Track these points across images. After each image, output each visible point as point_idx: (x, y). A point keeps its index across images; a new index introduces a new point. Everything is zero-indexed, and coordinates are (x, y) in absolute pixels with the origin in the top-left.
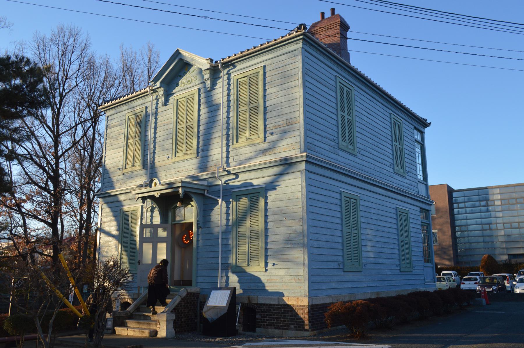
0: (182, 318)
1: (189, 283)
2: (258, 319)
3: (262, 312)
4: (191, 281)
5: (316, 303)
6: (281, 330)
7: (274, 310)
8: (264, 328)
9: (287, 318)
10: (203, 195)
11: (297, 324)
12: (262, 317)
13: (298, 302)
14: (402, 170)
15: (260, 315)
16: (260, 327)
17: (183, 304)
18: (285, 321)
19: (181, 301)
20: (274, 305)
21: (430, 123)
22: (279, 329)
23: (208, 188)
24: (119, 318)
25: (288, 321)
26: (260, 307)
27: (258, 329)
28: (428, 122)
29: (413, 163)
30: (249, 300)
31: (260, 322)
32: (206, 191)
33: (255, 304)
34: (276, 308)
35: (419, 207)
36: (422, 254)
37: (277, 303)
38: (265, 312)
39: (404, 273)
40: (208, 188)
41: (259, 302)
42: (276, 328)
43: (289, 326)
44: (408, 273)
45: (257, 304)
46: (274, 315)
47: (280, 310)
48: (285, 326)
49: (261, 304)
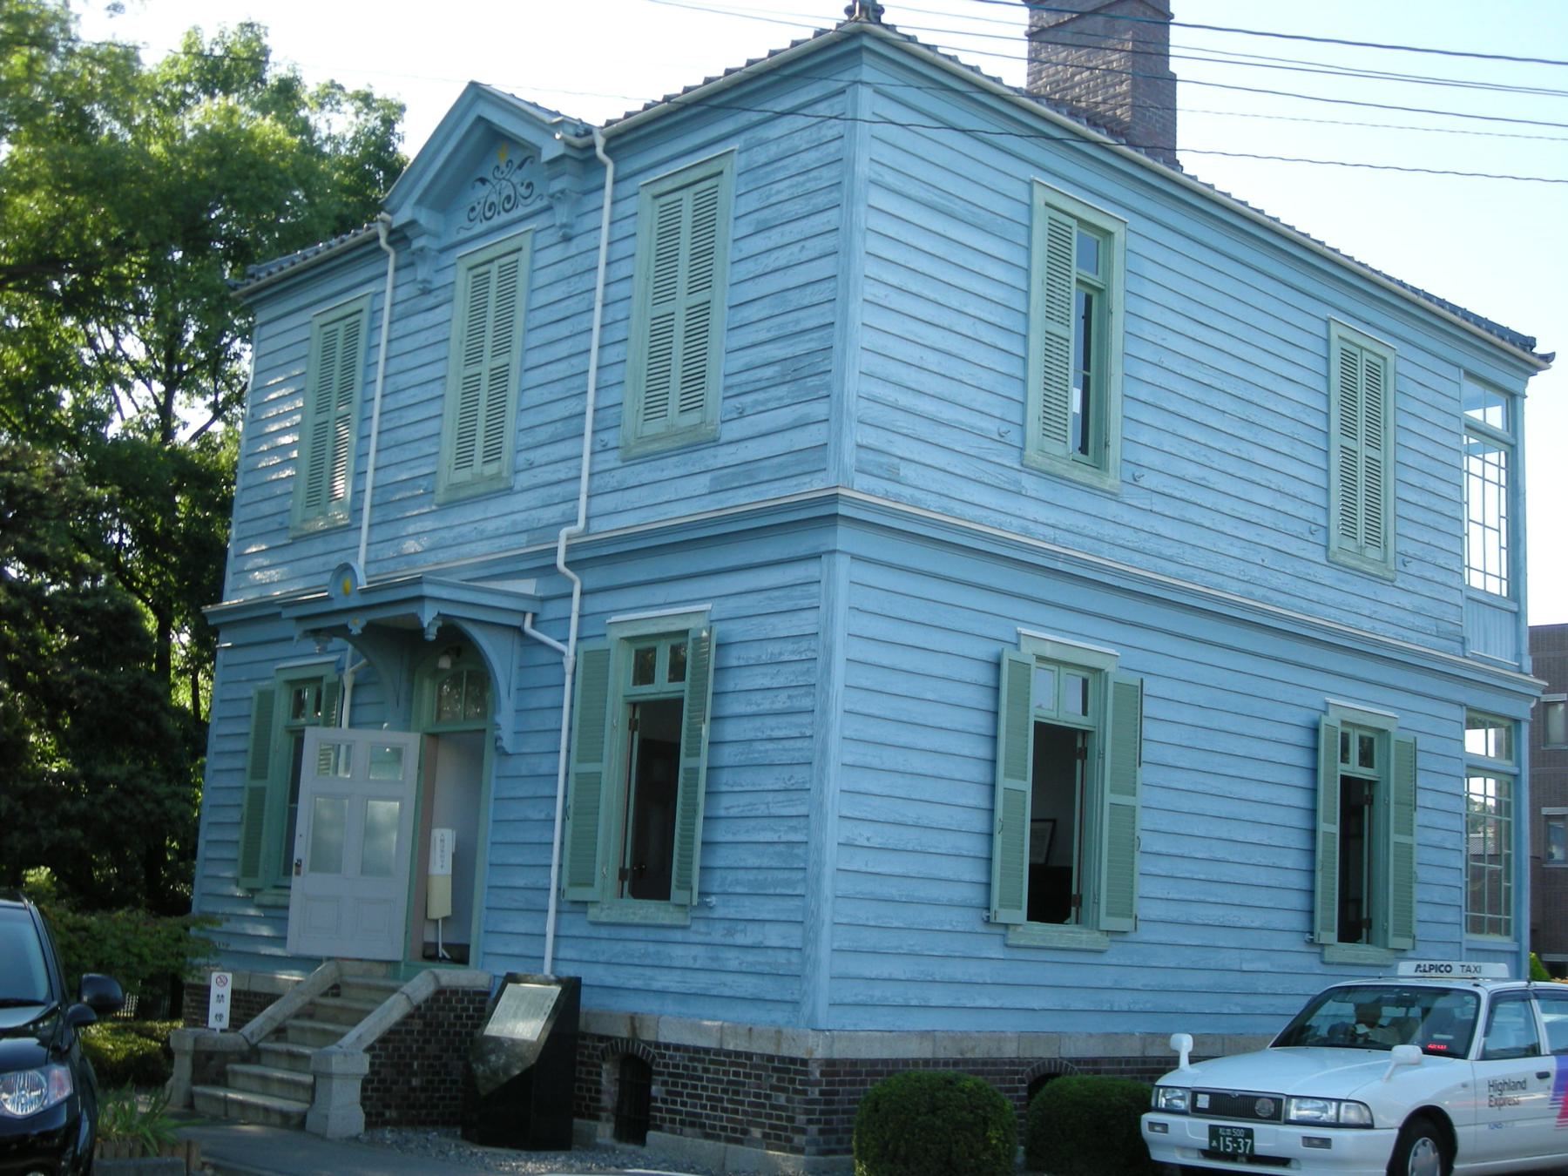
0: (415, 1074)
1: (460, 956)
2: (656, 1100)
3: (670, 1075)
4: (467, 947)
5: (851, 1054)
6: (723, 1144)
7: (706, 1070)
8: (673, 1132)
9: (742, 1103)
10: (519, 630)
11: (772, 1127)
12: (669, 1093)
13: (779, 1045)
14: (1372, 553)
15: (665, 1083)
16: (659, 1128)
17: (417, 1024)
18: (736, 1112)
19: (410, 1016)
20: (707, 1051)
21: (1548, 358)
22: (717, 1138)
23: (536, 608)
24: (210, 1055)
25: (745, 1113)
26: (663, 1056)
27: (652, 1135)
28: (1539, 349)
29: (1444, 524)
30: (634, 1028)
31: (660, 1109)
32: (529, 618)
33: (649, 1043)
34: (712, 1062)
35: (1461, 705)
36: (1460, 898)
37: (714, 1045)
38: (680, 1076)
39: (1019, 954)
40: (536, 608)
41: (661, 1040)
42: (707, 1136)
43: (745, 1132)
44: (1091, 958)
45: (658, 1045)
46: (704, 1088)
47: (726, 1073)
48: (734, 1130)
49: (667, 1046)
